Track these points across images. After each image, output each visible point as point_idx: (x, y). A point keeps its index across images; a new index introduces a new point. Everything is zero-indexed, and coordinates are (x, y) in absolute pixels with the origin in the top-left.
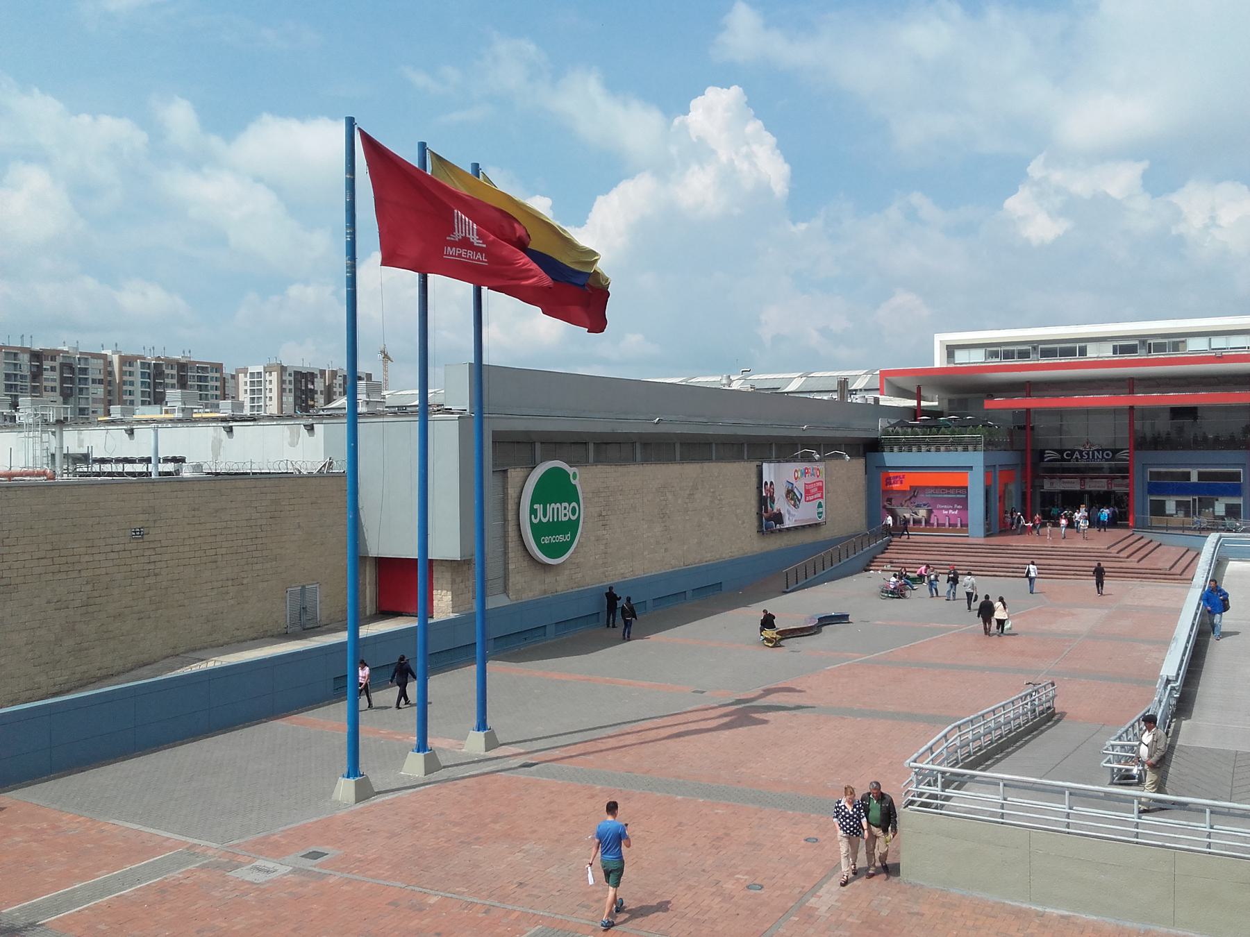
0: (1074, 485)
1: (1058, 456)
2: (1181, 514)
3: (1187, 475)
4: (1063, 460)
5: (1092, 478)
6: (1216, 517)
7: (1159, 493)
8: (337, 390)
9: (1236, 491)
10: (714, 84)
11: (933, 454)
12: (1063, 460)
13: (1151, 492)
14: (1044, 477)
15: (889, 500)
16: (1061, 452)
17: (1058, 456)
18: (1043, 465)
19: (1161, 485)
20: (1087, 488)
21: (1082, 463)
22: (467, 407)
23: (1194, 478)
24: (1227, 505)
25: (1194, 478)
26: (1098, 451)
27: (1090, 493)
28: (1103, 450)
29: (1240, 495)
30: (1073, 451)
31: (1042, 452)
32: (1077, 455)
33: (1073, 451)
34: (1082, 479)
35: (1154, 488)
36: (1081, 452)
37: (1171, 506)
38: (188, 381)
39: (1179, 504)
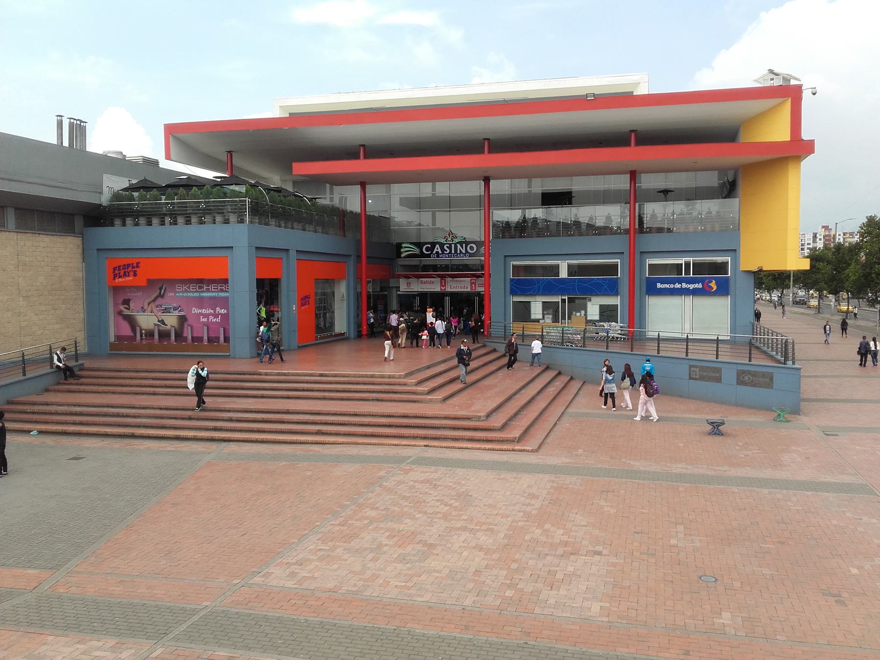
0: (433, 286)
1: (417, 251)
2: (549, 319)
3: (555, 269)
4: (423, 255)
5: (453, 276)
6: (588, 322)
7: (524, 293)
8: (559, 535)
9: (612, 289)
10: (806, 271)
11: (208, 228)
12: (423, 255)
13: (514, 293)
14: (399, 276)
15: (126, 302)
16: (419, 245)
17: (417, 251)
18: (401, 262)
19: (526, 282)
20: (448, 289)
21: (444, 260)
22: (81, 337)
23: (564, 274)
24: (601, 307)
25: (564, 274)
26: (461, 243)
27: (453, 295)
28: (467, 243)
29: (617, 294)
30: (433, 244)
31: (399, 246)
32: (437, 249)
33: (433, 244)
34: (442, 277)
35: (518, 287)
36: (442, 245)
37: (536, 310)
38: (41, 432)
39: (546, 306)
